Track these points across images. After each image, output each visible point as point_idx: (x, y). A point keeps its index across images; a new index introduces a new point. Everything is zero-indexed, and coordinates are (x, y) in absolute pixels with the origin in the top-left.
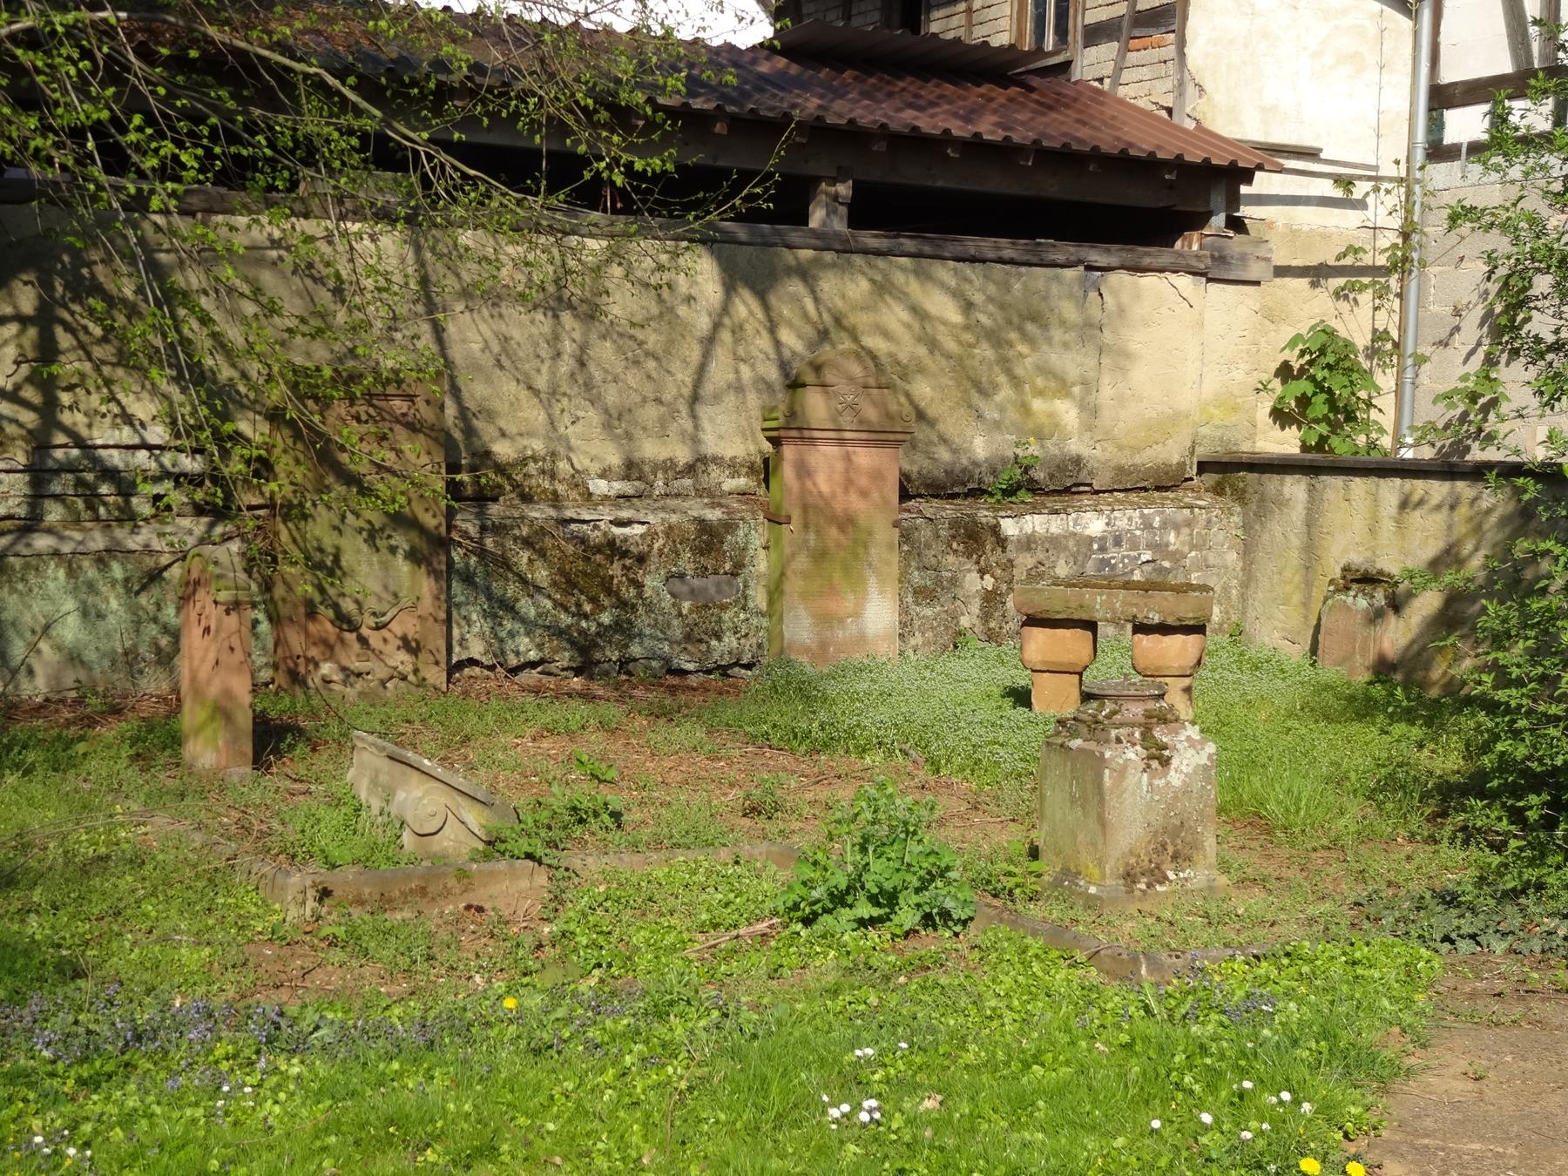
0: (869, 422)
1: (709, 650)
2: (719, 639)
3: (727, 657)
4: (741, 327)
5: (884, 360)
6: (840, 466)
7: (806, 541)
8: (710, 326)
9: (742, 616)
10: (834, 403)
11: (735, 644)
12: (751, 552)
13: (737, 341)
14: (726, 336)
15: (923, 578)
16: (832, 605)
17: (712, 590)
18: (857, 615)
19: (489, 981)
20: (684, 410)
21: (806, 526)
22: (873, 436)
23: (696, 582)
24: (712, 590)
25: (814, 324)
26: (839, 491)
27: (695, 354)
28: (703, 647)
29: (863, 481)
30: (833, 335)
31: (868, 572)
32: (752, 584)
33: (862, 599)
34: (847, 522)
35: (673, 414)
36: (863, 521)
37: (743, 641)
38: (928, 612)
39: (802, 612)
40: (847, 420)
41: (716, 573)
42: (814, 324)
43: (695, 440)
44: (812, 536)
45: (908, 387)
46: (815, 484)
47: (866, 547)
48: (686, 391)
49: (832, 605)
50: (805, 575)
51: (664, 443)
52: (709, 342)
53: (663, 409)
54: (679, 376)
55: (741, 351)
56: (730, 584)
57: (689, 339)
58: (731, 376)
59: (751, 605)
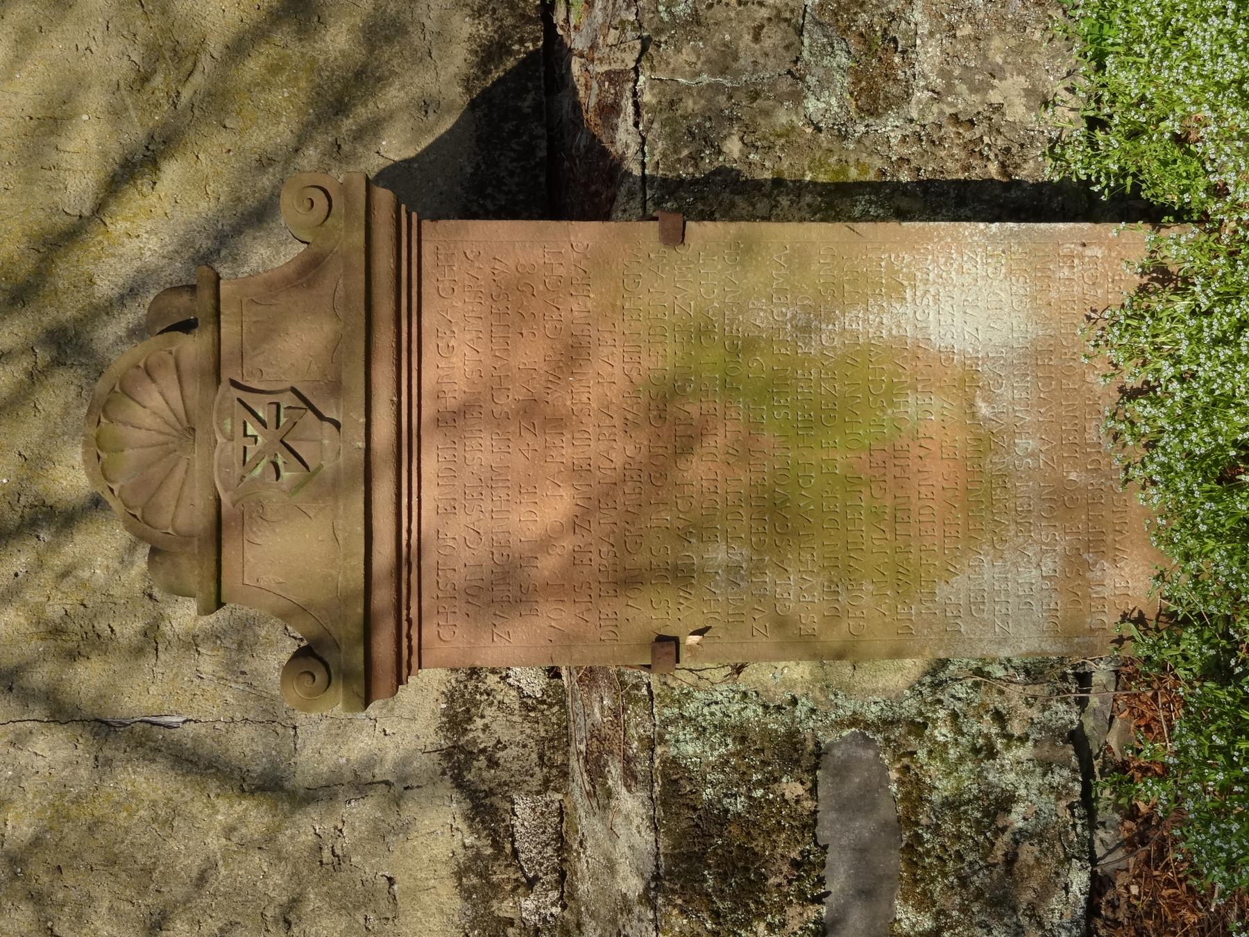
0: (336, 348)
1: (1037, 836)
2: (1005, 802)
3: (1059, 777)
4: (56, 631)
5: (135, 132)
6: (482, 450)
7: (733, 570)
8: (60, 734)
9: (942, 732)
10: (273, 495)
11: (1024, 752)
12: (752, 712)
13: (93, 643)
14: (87, 678)
15: (825, 84)
16: (935, 476)
17: (863, 827)
18: (968, 381)
19: (1214, 434)
20: (307, 827)
21: (682, 576)
22: (384, 339)
23: (838, 881)
24: (863, 827)
25: (35, 377)
26: (567, 451)
27: (146, 783)
28: (1028, 852)
29: (532, 354)
30: (67, 311)
31: (829, 338)
32: (848, 707)
33: (910, 363)
34: (670, 419)
35: (328, 862)
36: (662, 359)
37: (1016, 728)
38: (929, 56)
39: (955, 590)
40: (329, 449)
41: (810, 824)
42: (35, 377)
43: (397, 789)
44: (719, 554)
45: (215, 45)
46: (545, 543)
47: (743, 347)
48: (254, 816)
49: (935, 476)
50: (841, 574)
51: (413, 893)
52: (104, 729)
53: (313, 900)
54: (215, 843)
55: (128, 629)
56: (842, 771)
57: (102, 808)
58: (208, 663)
59: (910, 707)
